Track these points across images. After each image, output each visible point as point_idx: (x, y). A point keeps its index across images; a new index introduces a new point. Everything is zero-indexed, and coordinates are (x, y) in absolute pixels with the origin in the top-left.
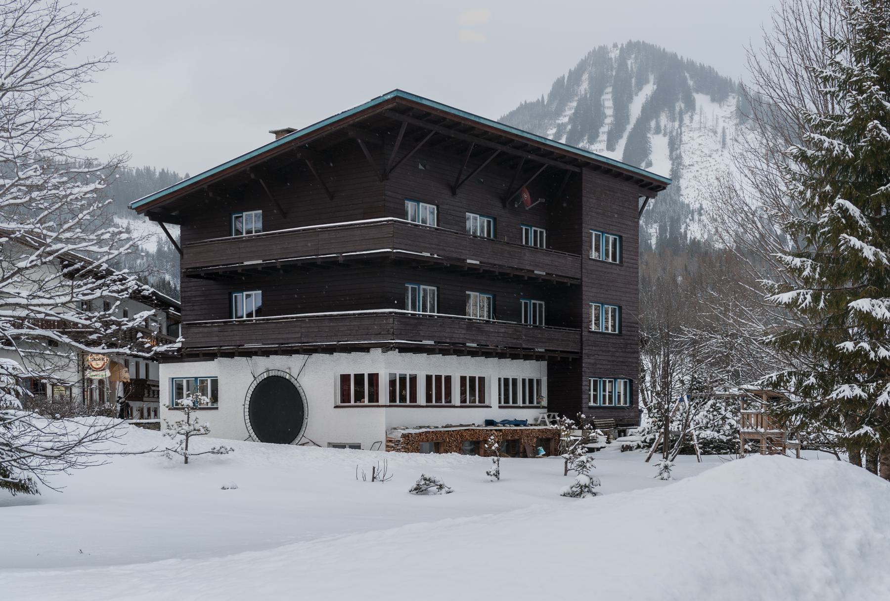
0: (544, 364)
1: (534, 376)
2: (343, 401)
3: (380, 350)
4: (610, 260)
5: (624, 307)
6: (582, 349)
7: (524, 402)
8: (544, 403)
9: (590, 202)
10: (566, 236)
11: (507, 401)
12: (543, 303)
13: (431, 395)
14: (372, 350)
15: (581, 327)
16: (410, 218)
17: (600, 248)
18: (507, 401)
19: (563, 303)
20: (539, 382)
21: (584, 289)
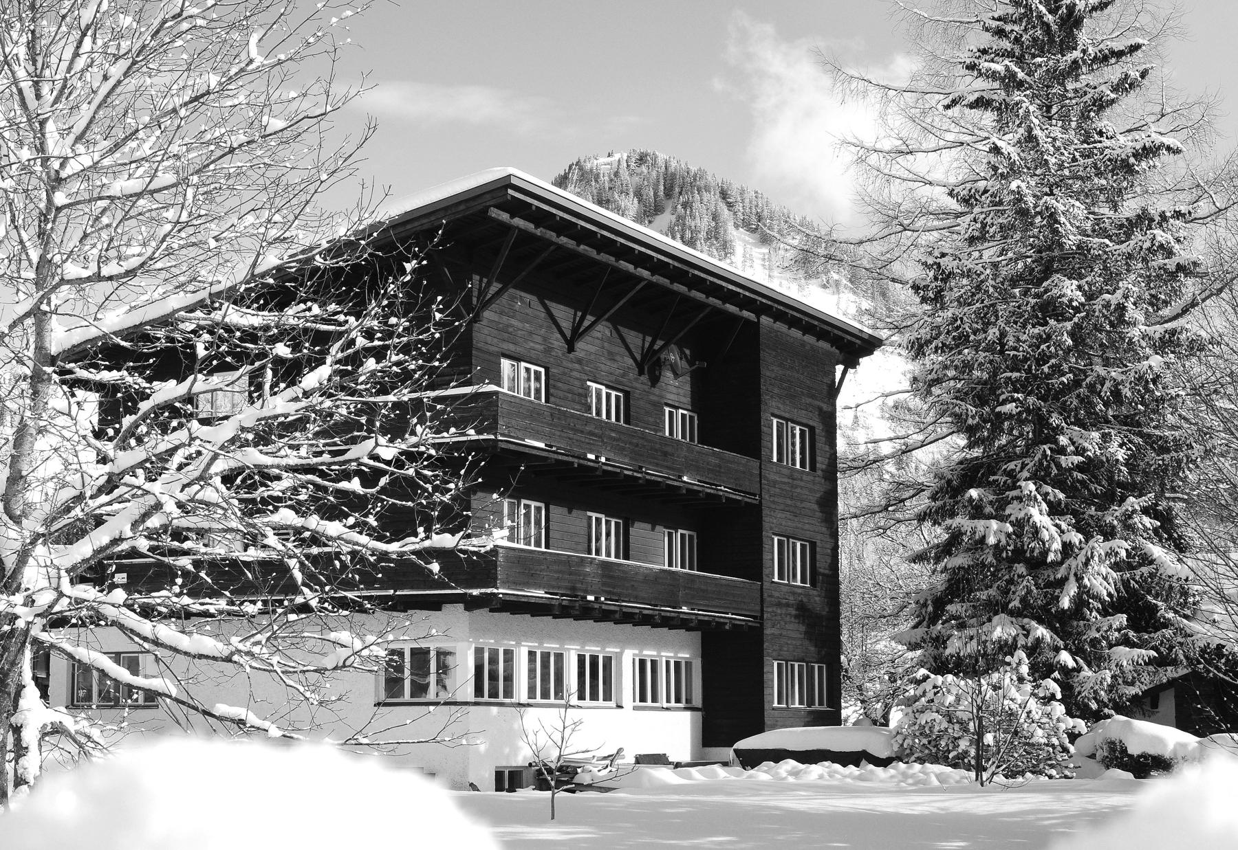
0: (697, 636)
1: (684, 655)
2: (561, 655)
3: (461, 606)
4: (798, 466)
5: (637, 393)
6: (762, 611)
7: (668, 701)
8: (697, 701)
9: (771, 369)
10: (729, 416)
11: (643, 699)
12: (695, 534)
13: (542, 680)
14: (448, 608)
15: (761, 579)
16: (506, 383)
17: (783, 440)
18: (643, 699)
19: (727, 534)
20: (689, 664)
21: (765, 512)
